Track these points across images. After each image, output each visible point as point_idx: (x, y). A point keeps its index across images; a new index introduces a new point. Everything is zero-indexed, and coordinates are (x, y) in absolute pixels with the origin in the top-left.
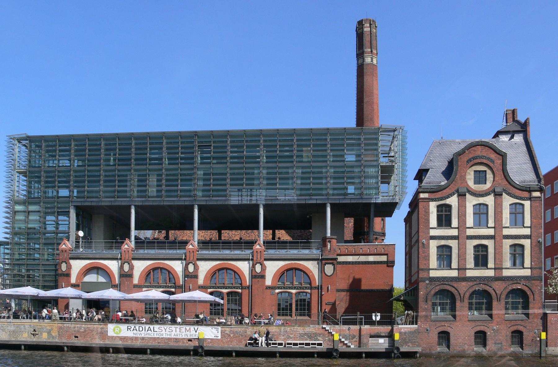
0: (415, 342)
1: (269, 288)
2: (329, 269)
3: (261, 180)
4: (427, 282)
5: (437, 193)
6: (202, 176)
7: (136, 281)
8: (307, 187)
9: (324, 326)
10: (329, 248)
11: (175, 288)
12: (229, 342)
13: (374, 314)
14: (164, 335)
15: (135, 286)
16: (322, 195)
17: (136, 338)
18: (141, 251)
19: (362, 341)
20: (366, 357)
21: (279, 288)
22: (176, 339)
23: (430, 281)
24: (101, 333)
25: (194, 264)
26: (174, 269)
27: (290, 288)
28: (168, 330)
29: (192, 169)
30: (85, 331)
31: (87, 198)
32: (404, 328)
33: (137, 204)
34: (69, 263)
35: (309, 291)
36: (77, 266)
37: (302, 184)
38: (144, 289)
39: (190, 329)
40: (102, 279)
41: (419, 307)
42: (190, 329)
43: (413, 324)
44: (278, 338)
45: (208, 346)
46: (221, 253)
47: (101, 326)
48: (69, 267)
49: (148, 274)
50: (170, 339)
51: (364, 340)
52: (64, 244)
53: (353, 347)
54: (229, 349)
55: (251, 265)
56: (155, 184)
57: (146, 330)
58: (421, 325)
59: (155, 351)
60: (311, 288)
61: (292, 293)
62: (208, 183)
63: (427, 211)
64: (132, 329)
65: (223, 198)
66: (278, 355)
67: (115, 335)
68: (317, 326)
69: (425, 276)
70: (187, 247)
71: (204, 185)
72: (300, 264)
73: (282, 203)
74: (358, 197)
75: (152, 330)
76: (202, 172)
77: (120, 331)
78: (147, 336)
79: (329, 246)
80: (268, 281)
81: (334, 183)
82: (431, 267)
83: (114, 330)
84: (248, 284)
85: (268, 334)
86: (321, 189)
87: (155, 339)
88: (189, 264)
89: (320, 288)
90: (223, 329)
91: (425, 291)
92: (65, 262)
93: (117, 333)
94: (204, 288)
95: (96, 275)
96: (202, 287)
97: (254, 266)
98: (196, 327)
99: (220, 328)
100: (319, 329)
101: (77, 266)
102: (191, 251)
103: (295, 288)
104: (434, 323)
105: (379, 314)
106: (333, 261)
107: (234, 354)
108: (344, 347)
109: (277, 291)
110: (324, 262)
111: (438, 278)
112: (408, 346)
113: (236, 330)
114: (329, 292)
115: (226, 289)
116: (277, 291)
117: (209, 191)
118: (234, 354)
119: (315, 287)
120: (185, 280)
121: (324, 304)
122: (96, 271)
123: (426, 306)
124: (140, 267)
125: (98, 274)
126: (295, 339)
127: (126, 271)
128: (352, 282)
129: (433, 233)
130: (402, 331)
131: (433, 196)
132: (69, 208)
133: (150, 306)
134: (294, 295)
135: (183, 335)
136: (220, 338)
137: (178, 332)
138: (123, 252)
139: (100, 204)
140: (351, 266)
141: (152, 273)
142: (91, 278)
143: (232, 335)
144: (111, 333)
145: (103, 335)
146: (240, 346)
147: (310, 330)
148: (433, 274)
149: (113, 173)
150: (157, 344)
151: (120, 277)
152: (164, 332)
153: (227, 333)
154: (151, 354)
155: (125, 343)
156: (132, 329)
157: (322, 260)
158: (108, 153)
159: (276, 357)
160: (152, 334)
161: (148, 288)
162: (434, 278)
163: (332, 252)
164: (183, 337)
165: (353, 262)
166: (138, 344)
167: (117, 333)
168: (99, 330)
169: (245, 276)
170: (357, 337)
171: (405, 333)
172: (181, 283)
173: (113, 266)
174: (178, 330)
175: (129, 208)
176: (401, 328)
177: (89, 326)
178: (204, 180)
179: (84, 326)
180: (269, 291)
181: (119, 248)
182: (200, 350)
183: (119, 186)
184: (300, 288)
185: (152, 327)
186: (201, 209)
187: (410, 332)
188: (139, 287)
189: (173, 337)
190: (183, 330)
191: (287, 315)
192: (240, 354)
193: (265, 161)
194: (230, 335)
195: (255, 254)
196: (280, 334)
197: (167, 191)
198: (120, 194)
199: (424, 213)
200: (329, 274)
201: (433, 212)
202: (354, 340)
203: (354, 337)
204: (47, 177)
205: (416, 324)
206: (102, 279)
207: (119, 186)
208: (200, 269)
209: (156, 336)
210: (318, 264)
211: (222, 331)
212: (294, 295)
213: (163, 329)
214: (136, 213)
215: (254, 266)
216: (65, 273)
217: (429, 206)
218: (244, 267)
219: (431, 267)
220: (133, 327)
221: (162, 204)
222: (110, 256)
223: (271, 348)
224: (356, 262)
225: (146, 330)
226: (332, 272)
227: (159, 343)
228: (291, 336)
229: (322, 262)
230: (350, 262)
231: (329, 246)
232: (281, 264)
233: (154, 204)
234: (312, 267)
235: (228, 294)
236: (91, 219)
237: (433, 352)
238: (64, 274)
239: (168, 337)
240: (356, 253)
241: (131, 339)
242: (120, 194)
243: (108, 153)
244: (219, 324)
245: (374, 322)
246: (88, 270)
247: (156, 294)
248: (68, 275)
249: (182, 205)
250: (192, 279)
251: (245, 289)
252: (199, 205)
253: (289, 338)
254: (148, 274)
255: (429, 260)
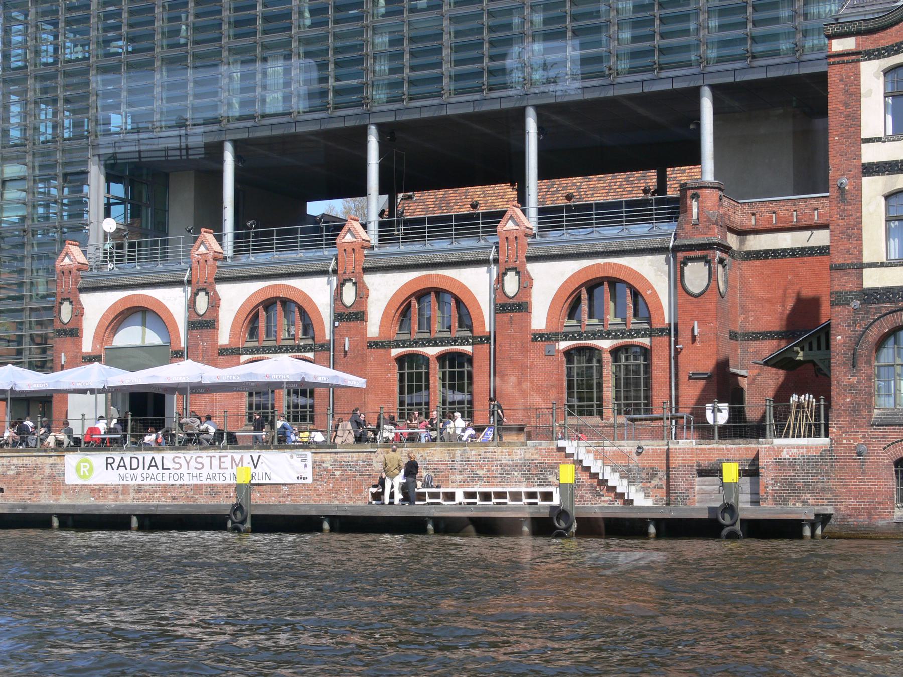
0: (823, 489)
1: (539, 337)
2: (696, 276)
3: (703, 17)
4: (856, 304)
5: (883, 34)
6: (386, 47)
7: (224, 337)
8: (738, 33)
9: (561, 443)
10: (695, 216)
11: (650, 336)
12: (329, 492)
13: (709, 406)
14: (186, 477)
15: (224, 351)
16: (688, 64)
17: (126, 488)
18: (552, 235)
19: (672, 488)
20: (658, 536)
21: (566, 337)
22: (212, 487)
23: (865, 302)
24: (52, 477)
25: (355, 284)
26: (166, 309)
27: (595, 335)
28: (193, 464)
29: (359, 33)
30: (18, 474)
31: (490, 90)
32: (789, 447)
33: (238, 136)
34: (79, 302)
35: (646, 341)
36: (97, 306)
37: (722, 27)
38: (244, 358)
39: (242, 459)
40: (153, 338)
41: (834, 383)
42: (242, 459)
43: (817, 435)
44: (447, 478)
45: (260, 502)
46: (429, 247)
47: (51, 461)
48: (78, 313)
49: (253, 319)
50: (197, 488)
51: (680, 485)
52: (202, 243)
53: (642, 501)
54: (314, 513)
55: (495, 276)
56: (282, 81)
57: (147, 466)
58: (842, 437)
59: (154, 522)
60: (650, 333)
61: (426, 359)
62: (646, 31)
63: (852, 89)
64: (115, 466)
65: (436, 101)
66: (430, 526)
67: (80, 482)
68: (545, 444)
69: (849, 287)
70: (500, 228)
71: (635, 39)
72: (621, 266)
73: (553, 101)
74: (786, 60)
75: (128, 467)
76: (386, 39)
77: (91, 470)
78: (148, 482)
79: (695, 210)
80: (539, 321)
81: (722, 27)
82: (866, 259)
83: (78, 470)
84: (667, 322)
85: (412, 469)
86: (687, 48)
87: (165, 489)
88: (505, 274)
89: (672, 332)
90: (318, 457)
91: (849, 332)
92: (68, 299)
93: (83, 477)
94: (383, 346)
95: (140, 328)
96: (376, 343)
97: (500, 280)
98: (255, 454)
99: (308, 454)
100: (549, 451)
101: (97, 306)
102: (349, 250)
103: (607, 335)
104: (880, 432)
105: (725, 406)
106: (701, 251)
107: (652, 529)
108: (618, 504)
109: (564, 345)
110: (681, 255)
111: (888, 290)
112: (804, 502)
113: (347, 458)
114: (698, 343)
115: (436, 345)
116: (564, 345)
117: (649, 52)
118: (652, 529)
119: (662, 331)
120: (334, 327)
121: (683, 378)
122: (139, 317)
123: (854, 380)
124: (235, 298)
125: (144, 324)
126: (489, 481)
127: (201, 312)
128: (794, 309)
129: (871, 154)
130: (785, 455)
131: (870, 42)
132: (85, 163)
133: (260, 403)
134: (607, 357)
135: (227, 475)
136: (309, 481)
137: (216, 470)
138: (195, 265)
139: (444, 113)
140: (787, 261)
141: (415, 305)
142: (131, 336)
143: (337, 473)
144: (71, 479)
145: (56, 481)
146: (356, 501)
147: (528, 456)
148: (872, 279)
149: (474, 24)
150: (169, 502)
151: (496, 313)
152: (184, 470)
153: (326, 469)
154: (142, 528)
155: (101, 502)
156: (115, 466)
157: (676, 249)
158: (174, 13)
159: (424, 531)
160: (159, 477)
161: (252, 352)
162: (876, 290)
163: (703, 225)
164: (228, 482)
165: (793, 250)
166: (110, 504)
167: (83, 477)
168: (47, 470)
169: (479, 307)
170: (662, 474)
171: (793, 462)
172: (487, 330)
173: (173, 301)
174: (215, 462)
175: (694, 95)
176: (781, 448)
177: (26, 461)
178: (636, 24)
179: (15, 461)
180: (541, 345)
181: (332, 243)
182: (727, 520)
183: (663, 36)
184: (623, 334)
185: (158, 456)
186: (387, 133)
187: (807, 460)
188: (230, 354)
189: (205, 482)
190: (227, 462)
191: (590, 413)
192: (348, 524)
193: (308, 22)
194: (333, 475)
195: (504, 246)
196: (453, 468)
197: (458, 77)
198: (665, 59)
199: (842, 97)
200: (696, 291)
201: (870, 92)
202: (655, 482)
203: (653, 474)
204: (457, 34)
205: (827, 436)
206: (153, 338)
207: (663, 36)
208: (373, 296)
209: (167, 482)
210: (667, 261)
211: (314, 462)
212: (607, 357)
213: (182, 461)
214: (541, 130)
215: (500, 280)
216: (68, 328)
217: (858, 75)
218: (476, 283)
219: (866, 259)
220: (118, 459)
221: (293, 131)
222: (167, 277)
223: (419, 508)
224: (802, 249)
225: (147, 466)
226: (705, 283)
227: (174, 499)
228: (481, 473)
229: (680, 254)
230: (784, 250)
231: (695, 210)
232: (569, 269)
233: (276, 133)
234: (652, 271)
235: (441, 358)
236: (167, 186)
237: (881, 523)
238: (65, 331)
239: (195, 482)
240: (803, 223)
241: (115, 490)
242: (665, 59)
243: (174, 13)
244: (306, 446)
245: (712, 428)
246: (122, 317)
247: (282, 368)
248: (74, 333)
249: (265, 138)
250: (352, 324)
251: (481, 342)
252: (381, 127)
253: (475, 478)
254: (405, 312)
255: (860, 238)
